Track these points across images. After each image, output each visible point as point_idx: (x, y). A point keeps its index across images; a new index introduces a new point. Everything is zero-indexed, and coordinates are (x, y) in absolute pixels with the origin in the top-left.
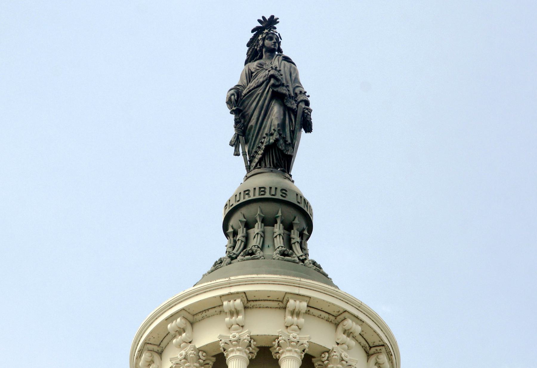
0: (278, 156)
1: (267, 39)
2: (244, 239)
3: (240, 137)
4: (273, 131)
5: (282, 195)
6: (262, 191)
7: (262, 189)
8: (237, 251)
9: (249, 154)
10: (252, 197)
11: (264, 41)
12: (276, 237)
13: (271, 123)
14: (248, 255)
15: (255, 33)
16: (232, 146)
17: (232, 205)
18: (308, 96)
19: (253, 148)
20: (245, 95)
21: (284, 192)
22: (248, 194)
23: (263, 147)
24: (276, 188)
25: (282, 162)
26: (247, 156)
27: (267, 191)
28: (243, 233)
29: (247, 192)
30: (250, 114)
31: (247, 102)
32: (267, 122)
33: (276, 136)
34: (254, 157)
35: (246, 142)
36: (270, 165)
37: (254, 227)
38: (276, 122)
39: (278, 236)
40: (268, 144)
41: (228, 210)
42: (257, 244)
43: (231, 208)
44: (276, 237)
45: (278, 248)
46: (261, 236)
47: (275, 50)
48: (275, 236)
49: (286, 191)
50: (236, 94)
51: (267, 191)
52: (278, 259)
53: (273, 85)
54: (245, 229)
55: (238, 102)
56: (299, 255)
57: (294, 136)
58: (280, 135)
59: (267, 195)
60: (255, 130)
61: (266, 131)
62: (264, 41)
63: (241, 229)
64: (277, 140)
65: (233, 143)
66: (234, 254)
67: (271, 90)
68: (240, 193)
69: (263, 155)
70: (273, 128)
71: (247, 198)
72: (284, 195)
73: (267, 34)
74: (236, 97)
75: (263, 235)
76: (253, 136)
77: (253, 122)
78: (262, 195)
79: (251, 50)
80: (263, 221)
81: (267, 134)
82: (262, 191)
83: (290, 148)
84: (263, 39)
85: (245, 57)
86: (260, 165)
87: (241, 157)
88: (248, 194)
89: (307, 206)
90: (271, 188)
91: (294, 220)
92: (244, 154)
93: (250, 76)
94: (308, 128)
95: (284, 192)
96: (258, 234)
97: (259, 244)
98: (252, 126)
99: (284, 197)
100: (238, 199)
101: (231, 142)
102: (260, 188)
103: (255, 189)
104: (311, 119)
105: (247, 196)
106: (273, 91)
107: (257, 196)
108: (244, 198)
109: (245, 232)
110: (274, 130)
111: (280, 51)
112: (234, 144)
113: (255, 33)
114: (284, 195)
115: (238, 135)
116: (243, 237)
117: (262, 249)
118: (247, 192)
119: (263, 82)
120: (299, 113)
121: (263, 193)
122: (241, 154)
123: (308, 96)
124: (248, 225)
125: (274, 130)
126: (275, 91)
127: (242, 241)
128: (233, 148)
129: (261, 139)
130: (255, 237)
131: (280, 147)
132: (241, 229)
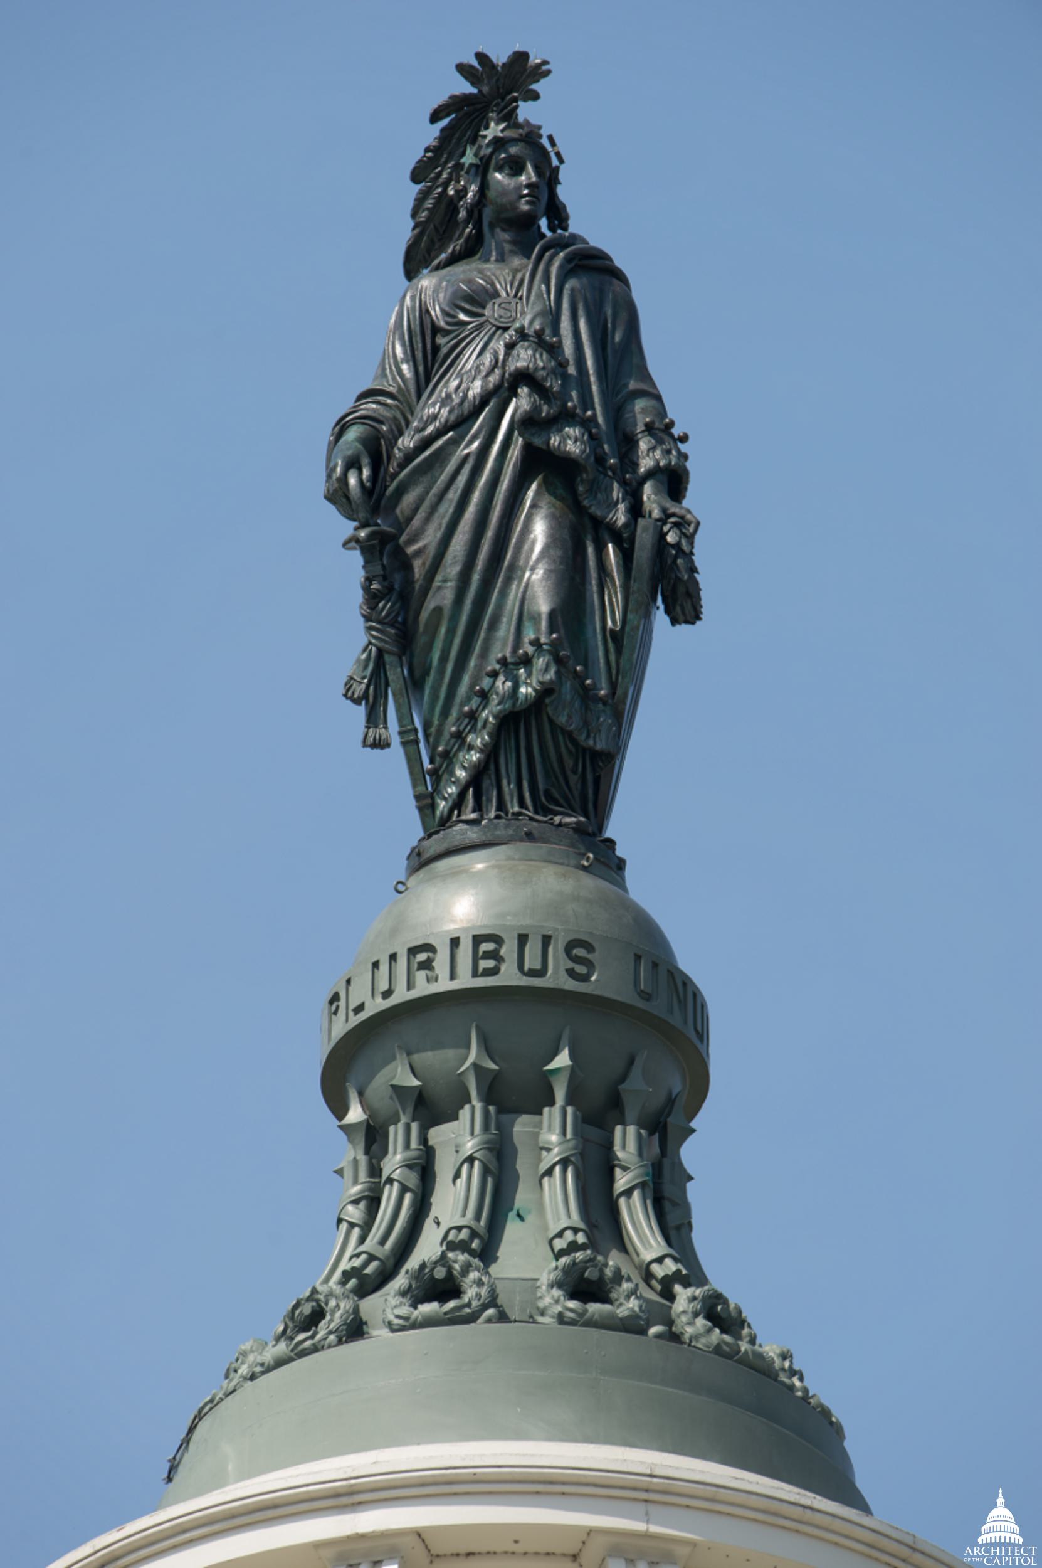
0: (551, 768)
1: (500, 169)
2: (413, 1180)
3: (388, 658)
4: (530, 650)
5: (571, 973)
6: (487, 955)
7: (485, 947)
8: (383, 1242)
9: (427, 736)
10: (444, 985)
11: (486, 178)
12: (549, 1172)
13: (525, 592)
14: (429, 1299)
15: (445, 122)
16: (357, 701)
17: (360, 1009)
18: (684, 439)
19: (445, 713)
20: (409, 457)
21: (579, 952)
22: (427, 965)
23: (488, 715)
24: (546, 940)
25: (574, 779)
26: (422, 745)
27: (508, 950)
28: (407, 1146)
29: (422, 957)
30: (432, 551)
31: (409, 499)
32: (504, 594)
33: (542, 671)
34: (446, 759)
35: (416, 682)
36: (522, 804)
37: (455, 1118)
38: (543, 605)
39: (558, 1169)
40: (508, 705)
41: (341, 1027)
42: (473, 1224)
43: (355, 1020)
44: (549, 1172)
45: (560, 1235)
46: (486, 1171)
47: (536, 223)
48: (544, 1167)
49: (590, 948)
50: (365, 461)
51: (508, 950)
52: (561, 1319)
53: (527, 423)
54: (414, 1126)
55: (378, 480)
56: (648, 1256)
57: (628, 648)
58: (558, 661)
59: (509, 976)
60: (451, 632)
61: (501, 649)
62: (486, 178)
63: (401, 1126)
64: (546, 692)
65: (359, 689)
66: (372, 1258)
67: (518, 442)
68: (393, 957)
69: (491, 754)
70: (529, 635)
71: (423, 987)
72: (581, 969)
73: (499, 143)
74: (366, 473)
75: (493, 1166)
76: (444, 659)
77: (443, 595)
78: (489, 972)
79: (429, 204)
80: (490, 1095)
81: (503, 662)
82: (487, 955)
83: (605, 719)
84: (482, 169)
85: (403, 230)
86: (478, 807)
87: (396, 751)
88: (427, 965)
89: (683, 1003)
90: (523, 939)
91: (623, 1078)
92: (410, 744)
93: (431, 348)
94: (685, 606)
95: (579, 952)
96: (470, 1160)
97: (478, 1217)
98: (438, 610)
99: (585, 978)
100: (383, 986)
101: (348, 687)
102: (477, 940)
103: (455, 942)
104: (693, 570)
105: (421, 976)
106: (528, 448)
107: (465, 980)
108: (410, 986)
109: (414, 1144)
110: (536, 643)
111: (557, 214)
112: (365, 696)
113: (445, 122)
114: (581, 969)
115: (380, 652)
116: (409, 1167)
117: (487, 1254)
118: (422, 957)
119: (484, 400)
120: (644, 538)
121: (490, 963)
122: (396, 740)
123: (684, 439)
124: (429, 1108)
125: (536, 643)
126: (538, 449)
127: (404, 1189)
128: (361, 711)
129: (475, 680)
130: (457, 1175)
131: (562, 720)
132: (401, 1126)
